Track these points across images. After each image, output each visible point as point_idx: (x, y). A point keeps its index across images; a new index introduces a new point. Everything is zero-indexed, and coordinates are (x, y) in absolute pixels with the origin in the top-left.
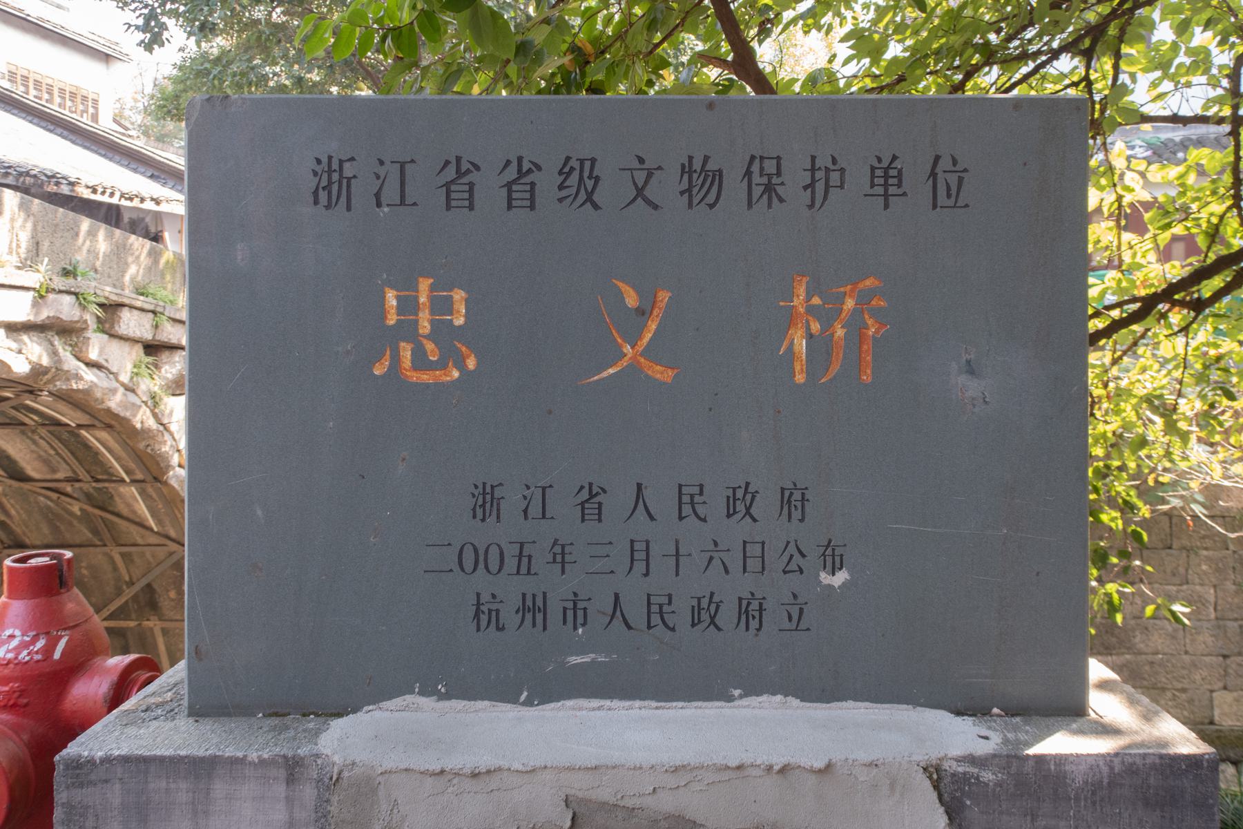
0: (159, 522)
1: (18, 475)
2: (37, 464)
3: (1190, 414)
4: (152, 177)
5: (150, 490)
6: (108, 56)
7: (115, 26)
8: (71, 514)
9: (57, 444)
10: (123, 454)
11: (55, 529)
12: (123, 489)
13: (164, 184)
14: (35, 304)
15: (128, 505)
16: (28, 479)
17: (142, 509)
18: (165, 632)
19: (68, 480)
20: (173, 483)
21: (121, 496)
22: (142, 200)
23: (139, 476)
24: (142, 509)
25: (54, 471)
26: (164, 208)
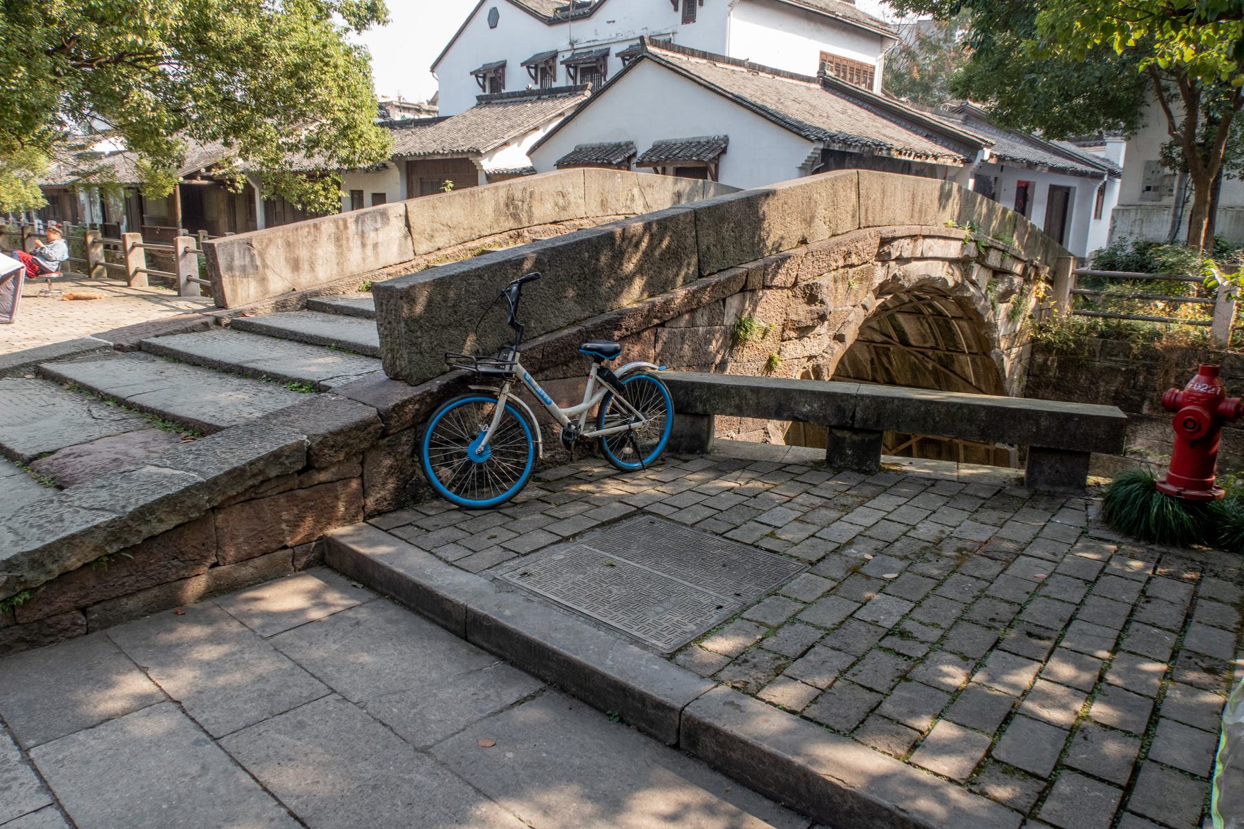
0: (977, 380)
1: (904, 341)
2: (918, 337)
3: (1164, 479)
4: (926, 137)
5: (978, 360)
6: (882, 36)
7: (885, 14)
8: (927, 369)
9: (935, 327)
10: (970, 336)
11: (915, 377)
12: (962, 357)
13: (936, 142)
14: (963, 248)
15: (962, 367)
16: (909, 345)
17: (970, 371)
18: (965, 447)
19: (932, 348)
20: (993, 357)
21: (959, 361)
22: (927, 157)
23: (975, 350)
24: (970, 371)
25: (925, 342)
26: (941, 161)
